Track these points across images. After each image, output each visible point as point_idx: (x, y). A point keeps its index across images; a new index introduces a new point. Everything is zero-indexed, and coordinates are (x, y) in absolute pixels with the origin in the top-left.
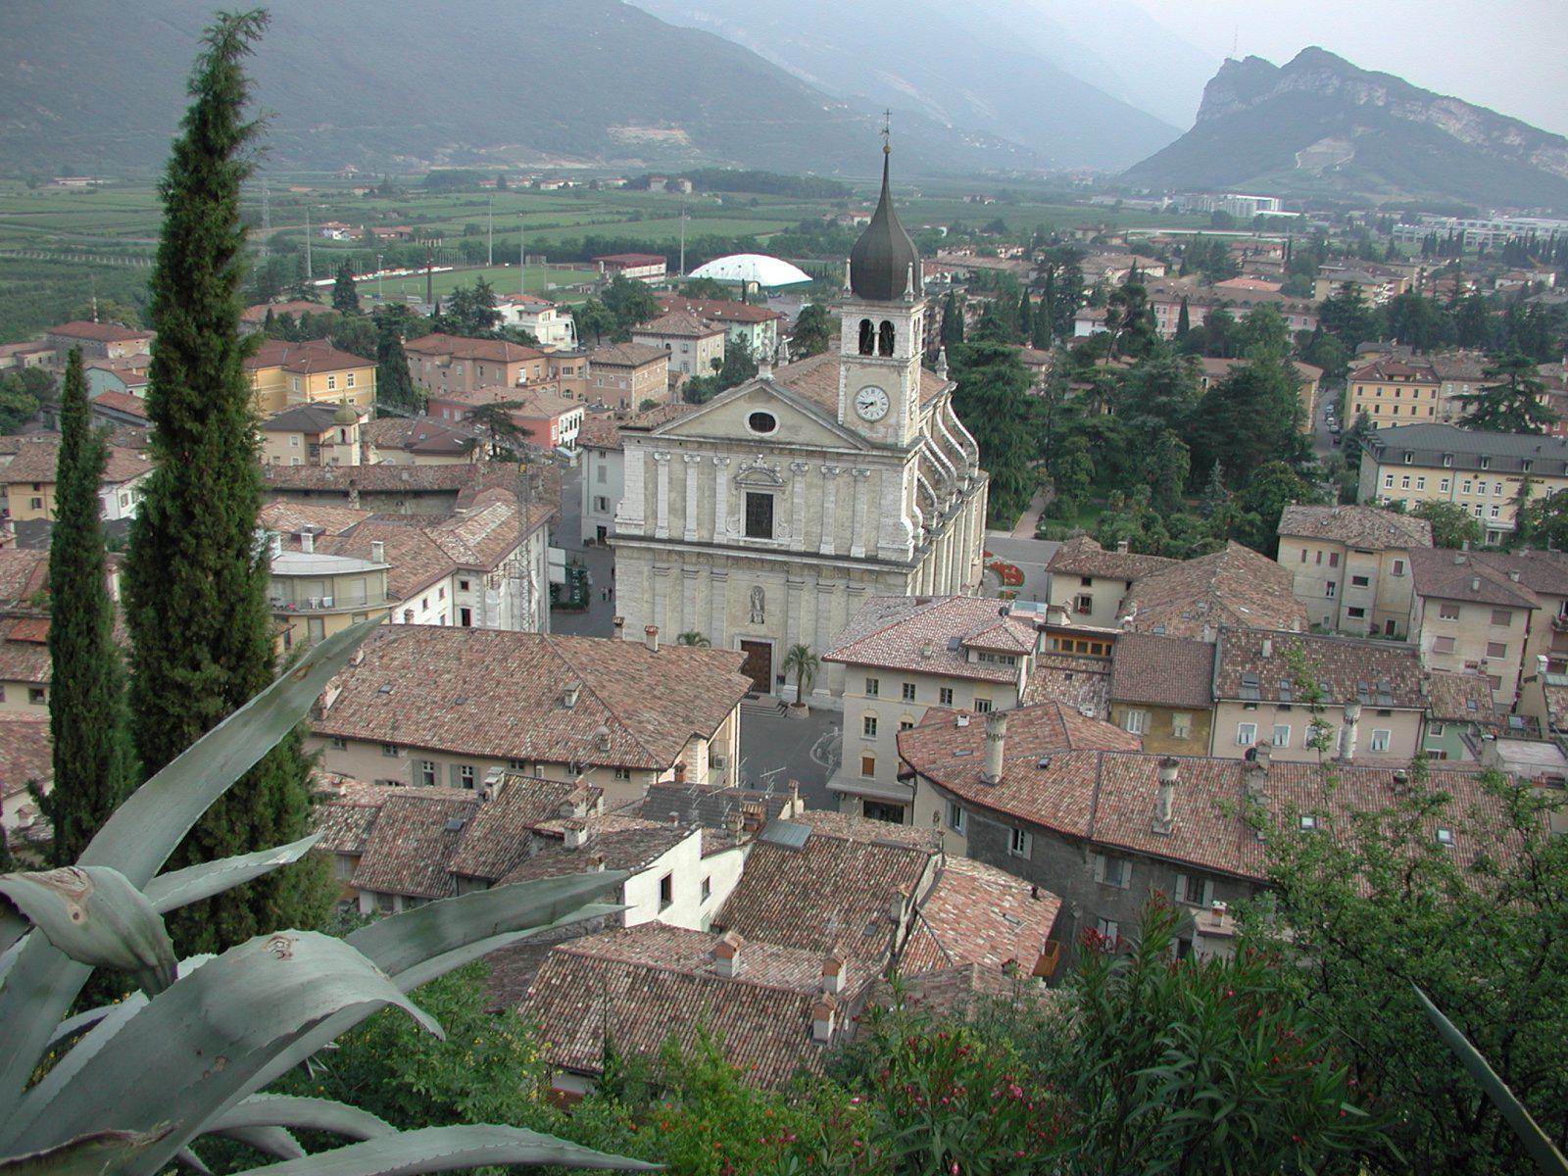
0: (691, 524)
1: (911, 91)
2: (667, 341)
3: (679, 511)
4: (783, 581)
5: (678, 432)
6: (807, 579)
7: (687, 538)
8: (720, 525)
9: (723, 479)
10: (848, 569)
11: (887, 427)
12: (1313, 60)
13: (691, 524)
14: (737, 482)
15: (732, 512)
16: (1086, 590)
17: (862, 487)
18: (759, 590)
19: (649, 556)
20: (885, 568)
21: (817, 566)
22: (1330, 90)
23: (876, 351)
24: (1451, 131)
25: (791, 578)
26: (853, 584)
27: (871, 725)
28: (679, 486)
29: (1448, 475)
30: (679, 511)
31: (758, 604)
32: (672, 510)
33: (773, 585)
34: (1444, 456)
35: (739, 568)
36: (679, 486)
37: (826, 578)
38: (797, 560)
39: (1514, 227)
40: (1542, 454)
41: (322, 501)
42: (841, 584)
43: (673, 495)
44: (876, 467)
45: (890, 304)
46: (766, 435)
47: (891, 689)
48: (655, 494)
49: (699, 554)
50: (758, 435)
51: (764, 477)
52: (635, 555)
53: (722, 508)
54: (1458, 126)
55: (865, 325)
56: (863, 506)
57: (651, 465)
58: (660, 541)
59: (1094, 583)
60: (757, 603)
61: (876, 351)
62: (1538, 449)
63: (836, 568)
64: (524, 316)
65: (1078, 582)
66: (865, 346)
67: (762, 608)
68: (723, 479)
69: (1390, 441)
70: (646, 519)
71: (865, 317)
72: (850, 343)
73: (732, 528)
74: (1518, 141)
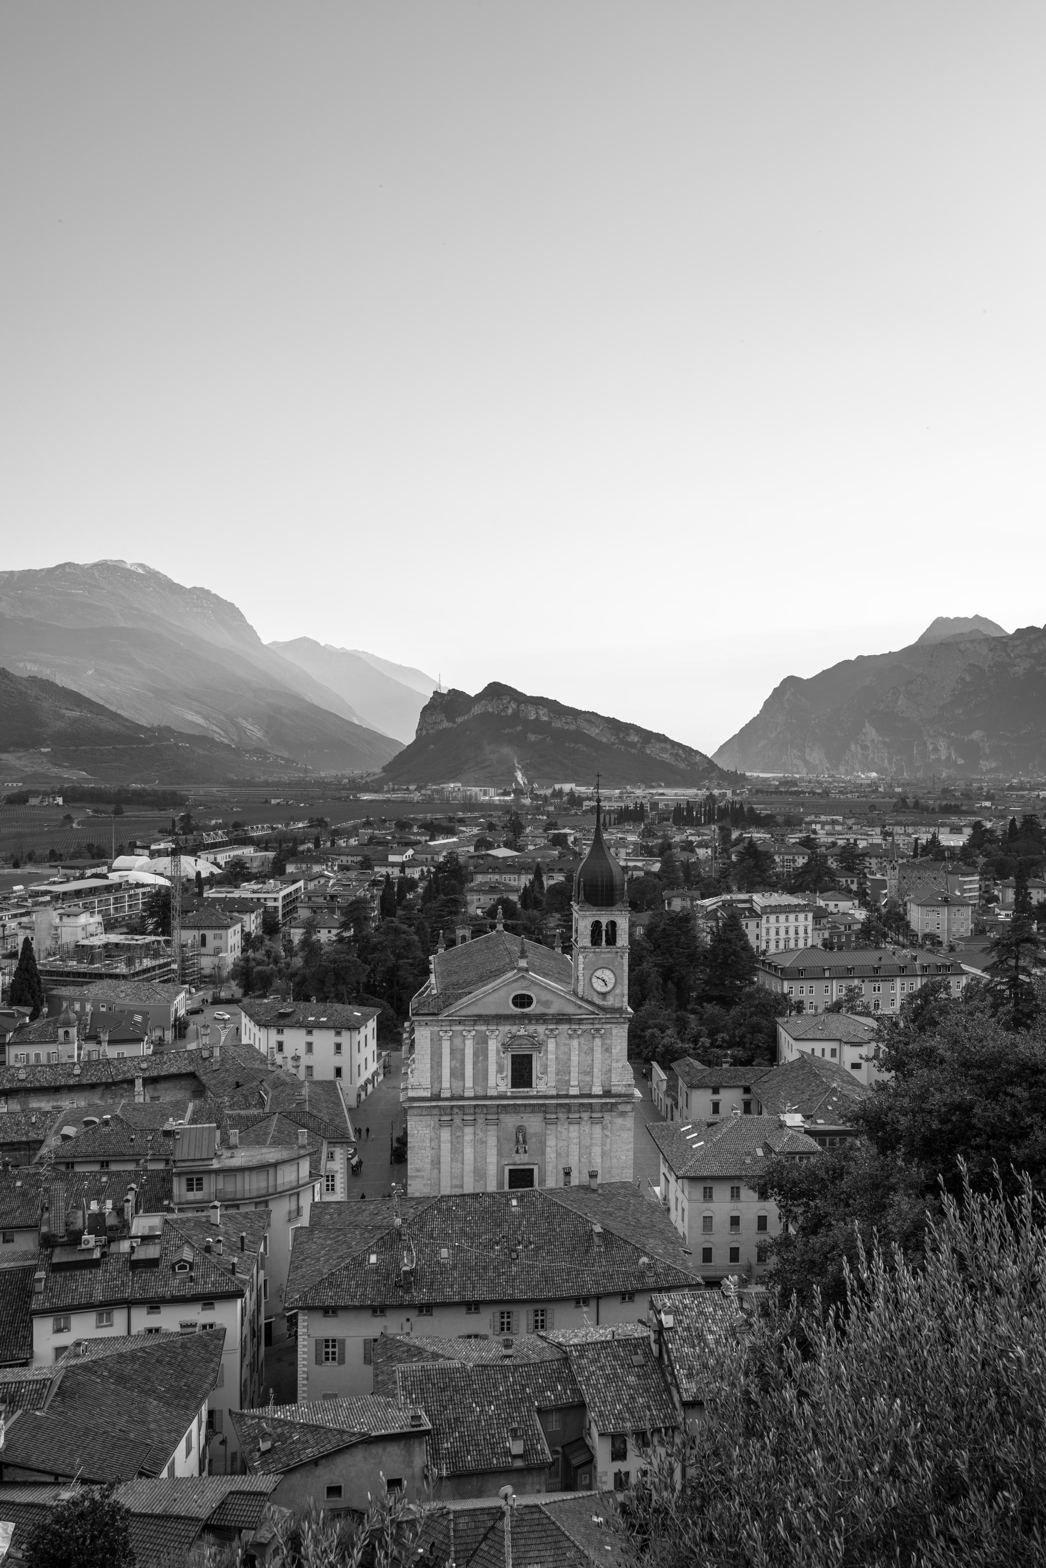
0: (469, 1083)
1: (200, 721)
2: (202, 932)
3: (457, 1073)
4: (541, 1119)
5: (458, 1014)
6: (560, 1115)
7: (467, 1094)
8: (492, 1081)
9: (493, 1045)
10: (591, 1104)
11: (615, 996)
12: (496, 691)
13: (469, 1083)
14: (506, 1047)
15: (500, 1070)
16: (716, 1097)
17: (598, 1042)
18: (520, 1129)
19: (436, 1111)
20: (620, 1100)
21: (567, 1104)
22: (510, 711)
23: (604, 943)
24: (593, 735)
25: (548, 1116)
26: (594, 1115)
27: (735, 1221)
28: (457, 1054)
29: (828, 983)
30: (457, 1073)
31: (521, 1139)
32: (453, 1074)
33: (533, 1123)
34: (824, 970)
35: (507, 1113)
36: (457, 1054)
37: (575, 1112)
38: (576, 1101)
39: (649, 796)
40: (883, 962)
41: (72, 1095)
42: (585, 1116)
43: (454, 1062)
44: (608, 1026)
45: (614, 908)
46: (526, 1010)
47: (722, 1192)
48: (439, 1064)
49: (476, 1106)
50: (519, 1010)
51: (525, 1042)
52: (424, 1113)
53: (492, 1068)
54: (597, 731)
55: (597, 925)
56: (598, 1055)
57: (436, 1043)
58: (492, 1098)
59: (721, 1091)
60: (521, 1139)
61: (604, 943)
62: (880, 959)
63: (582, 1104)
64: (65, 919)
65: (710, 1091)
66: (595, 941)
67: (525, 1142)
68: (493, 1045)
69: (787, 962)
70: (432, 1083)
71: (597, 919)
72: (583, 939)
73: (499, 1082)
74: (636, 739)
